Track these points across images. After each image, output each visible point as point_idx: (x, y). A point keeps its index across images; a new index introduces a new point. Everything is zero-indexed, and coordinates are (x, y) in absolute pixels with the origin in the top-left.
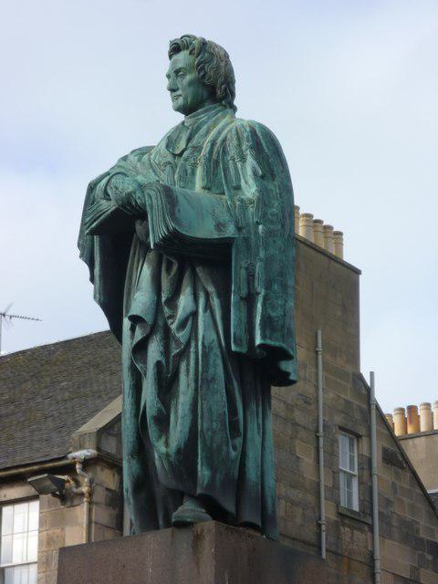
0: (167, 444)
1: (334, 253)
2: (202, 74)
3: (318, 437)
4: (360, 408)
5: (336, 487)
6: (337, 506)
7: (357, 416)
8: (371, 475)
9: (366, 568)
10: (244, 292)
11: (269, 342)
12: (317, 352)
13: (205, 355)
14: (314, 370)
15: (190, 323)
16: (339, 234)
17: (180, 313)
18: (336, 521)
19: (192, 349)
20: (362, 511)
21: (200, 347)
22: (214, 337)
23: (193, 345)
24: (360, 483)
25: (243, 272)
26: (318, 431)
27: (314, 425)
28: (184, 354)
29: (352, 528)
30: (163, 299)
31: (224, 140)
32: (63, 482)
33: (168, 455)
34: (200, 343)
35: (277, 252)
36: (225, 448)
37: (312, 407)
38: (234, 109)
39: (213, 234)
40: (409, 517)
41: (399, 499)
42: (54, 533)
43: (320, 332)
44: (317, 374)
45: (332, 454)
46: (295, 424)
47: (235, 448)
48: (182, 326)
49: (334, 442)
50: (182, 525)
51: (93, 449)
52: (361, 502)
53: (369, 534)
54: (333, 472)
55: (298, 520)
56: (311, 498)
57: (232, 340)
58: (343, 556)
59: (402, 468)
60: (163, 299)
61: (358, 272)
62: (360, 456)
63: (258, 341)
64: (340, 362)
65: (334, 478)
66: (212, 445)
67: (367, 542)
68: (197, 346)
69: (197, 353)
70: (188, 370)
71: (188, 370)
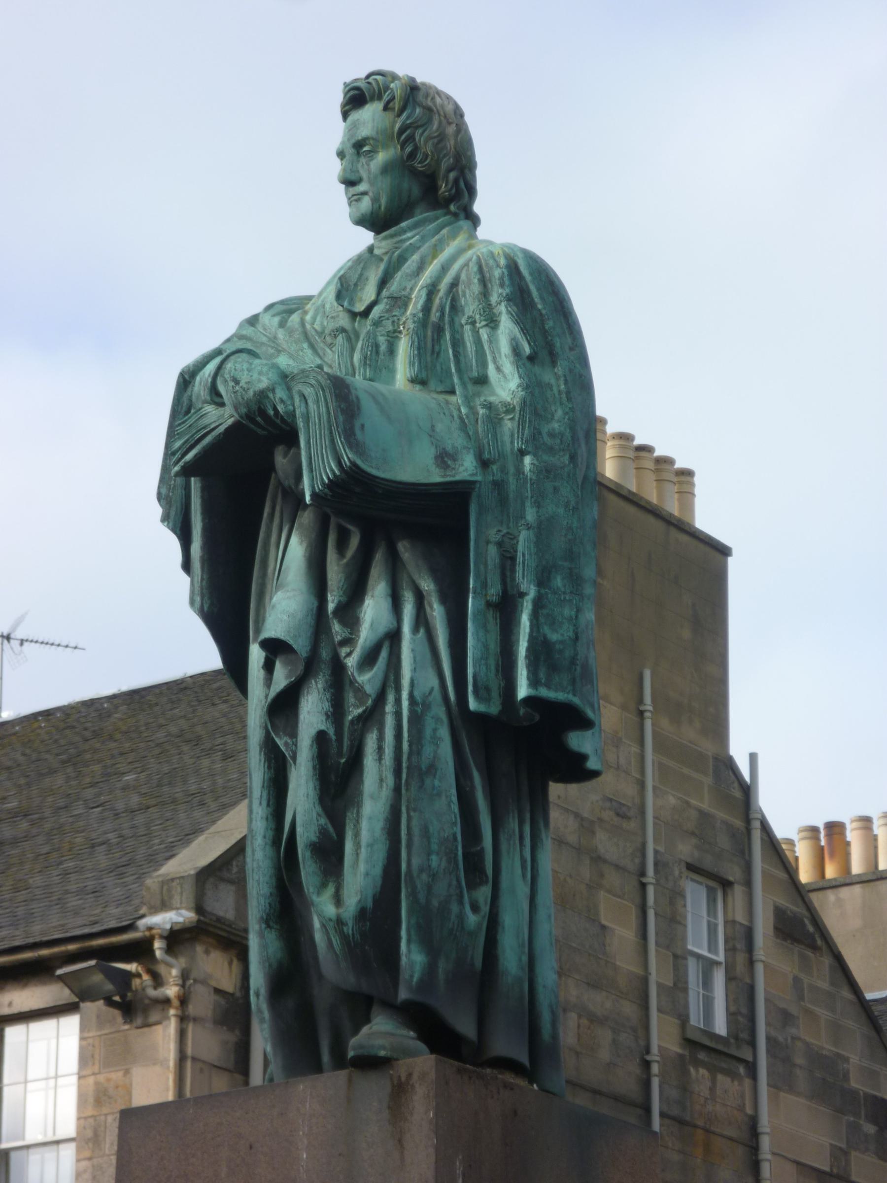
0: (338, 900)
1: (676, 513)
3: (643, 886)
5: (680, 985)
7: (724, 842)
8: (751, 963)
9: (740, 1151)
10: (494, 591)
11: (544, 692)
13: (416, 719)
14: (635, 749)
16: (687, 474)
17: (366, 635)
18: (681, 1056)
19: (389, 708)
20: (734, 1033)
21: (405, 704)
22: (434, 682)
23: (391, 698)
24: (730, 978)
25: (492, 552)
26: (643, 874)
27: (637, 861)
29: (713, 1070)
30: (331, 606)
31: (454, 284)
32: (129, 975)
33: (340, 922)
34: (405, 695)
35: (561, 511)
36: (455, 908)
37: (632, 825)
38: (475, 221)
39: (436, 477)
40: (825, 1044)
42: (108, 1080)
43: (647, 674)
44: (642, 758)
46: (597, 859)
47: (475, 908)
48: (369, 659)
49: (676, 896)
51: (188, 909)
52: (731, 1016)
53: (747, 1082)
54: (675, 956)
55: (605, 1054)
56: (629, 1009)
57: (470, 688)
58: (695, 1126)
59: (814, 948)
63: (523, 691)
68: (398, 701)
69: (398, 715)
70: (380, 749)
71: (380, 749)
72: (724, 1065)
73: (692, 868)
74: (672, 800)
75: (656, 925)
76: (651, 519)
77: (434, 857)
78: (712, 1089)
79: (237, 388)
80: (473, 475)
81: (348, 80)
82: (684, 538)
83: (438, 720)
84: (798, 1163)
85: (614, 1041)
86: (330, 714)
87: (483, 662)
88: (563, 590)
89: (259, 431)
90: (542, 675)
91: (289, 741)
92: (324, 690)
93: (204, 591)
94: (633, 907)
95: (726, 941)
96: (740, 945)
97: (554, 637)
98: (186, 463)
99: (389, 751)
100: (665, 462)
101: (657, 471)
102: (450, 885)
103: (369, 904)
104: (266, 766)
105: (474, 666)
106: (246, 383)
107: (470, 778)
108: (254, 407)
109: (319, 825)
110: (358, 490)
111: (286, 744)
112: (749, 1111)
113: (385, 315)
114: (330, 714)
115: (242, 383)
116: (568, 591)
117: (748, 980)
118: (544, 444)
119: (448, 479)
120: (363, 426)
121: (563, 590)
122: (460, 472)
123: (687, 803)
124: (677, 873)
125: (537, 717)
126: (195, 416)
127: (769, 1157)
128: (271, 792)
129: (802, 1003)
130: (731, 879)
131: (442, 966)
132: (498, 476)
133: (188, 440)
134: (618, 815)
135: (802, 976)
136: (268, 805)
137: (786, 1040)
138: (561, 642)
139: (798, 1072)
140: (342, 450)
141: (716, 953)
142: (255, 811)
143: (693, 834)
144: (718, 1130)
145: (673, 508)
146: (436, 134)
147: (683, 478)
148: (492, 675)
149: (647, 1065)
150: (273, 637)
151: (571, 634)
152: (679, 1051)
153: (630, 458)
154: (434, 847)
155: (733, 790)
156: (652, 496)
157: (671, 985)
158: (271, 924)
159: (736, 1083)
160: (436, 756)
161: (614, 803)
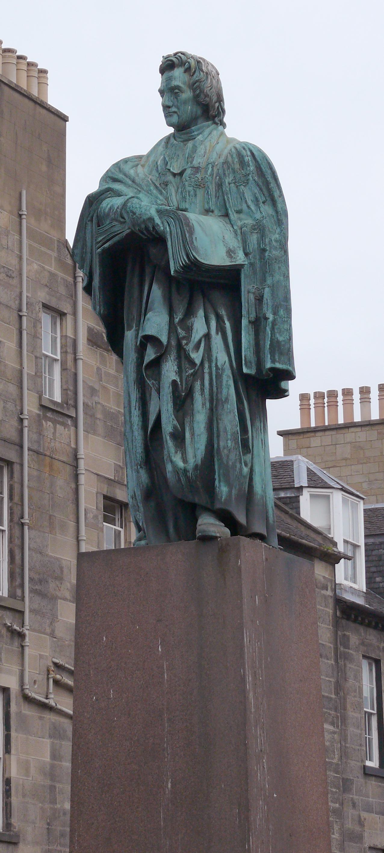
1: (15, 81)
2: (198, 92)
3: (20, 317)
4: (65, 280)
5: (38, 375)
6: (40, 398)
7: (62, 290)
8: (75, 360)
9: (68, 468)
10: (253, 316)
11: (273, 366)
12: (20, 216)
14: (17, 237)
15: (203, 344)
16: (44, 72)
18: (39, 415)
19: (206, 370)
20: (65, 402)
21: (214, 369)
22: (226, 359)
23: (206, 365)
24: (64, 369)
26: (20, 310)
27: (17, 302)
28: (198, 374)
29: (55, 422)
30: (177, 320)
34: (213, 365)
35: (282, 278)
36: (238, 465)
37: (15, 282)
38: (223, 125)
39: (227, 262)
41: (104, 387)
43: (24, 193)
44: (21, 242)
45: (35, 337)
47: (246, 465)
49: (36, 322)
50: (207, 539)
52: (64, 391)
53: (73, 429)
54: (36, 357)
56: (12, 389)
57: (243, 362)
58: (45, 455)
60: (177, 320)
61: (65, 119)
62: (64, 337)
64: (44, 227)
65: (36, 365)
66: (228, 462)
67: (70, 438)
68: (210, 367)
69: (210, 374)
70: (202, 390)
71: (202, 390)
72: (61, 420)
73: (46, 307)
74: (36, 267)
75: (27, 339)
76: (26, 101)
77: (229, 442)
78: (54, 433)
79: (134, 216)
80: (243, 261)
81: (165, 55)
82: (44, 111)
83: (228, 376)
84: (98, 475)
85: (4, 407)
86: (177, 372)
87: (248, 349)
88: (283, 316)
89: (143, 236)
90: (277, 357)
91: (154, 382)
92: (174, 360)
93: (101, 303)
94: (15, 329)
95: (61, 348)
96: (70, 350)
97: (281, 339)
98: (104, 248)
99: (207, 391)
100: (32, 65)
101: (39, 78)
102: (236, 455)
103: (199, 462)
104: (137, 391)
105: (245, 352)
106: (139, 214)
107: (243, 403)
108: (143, 226)
109: (173, 424)
110: (194, 269)
111: (153, 384)
112: (73, 446)
113: (191, 176)
114: (177, 372)
115: (137, 214)
116: (286, 316)
117: (73, 370)
118: (274, 246)
119: (233, 263)
120: (196, 238)
121: (283, 316)
122: (238, 260)
123: (43, 267)
124: (37, 308)
125: (272, 375)
126: (109, 225)
127: (84, 472)
128: (140, 403)
129: (101, 382)
130: (65, 311)
131: (234, 492)
132: (252, 261)
133: (105, 237)
134: (7, 276)
135: (101, 367)
136: (139, 410)
137: (93, 404)
138: (284, 341)
139: (98, 422)
140: (189, 251)
141: (56, 355)
142: (132, 412)
143: (46, 286)
144: (57, 457)
145: (35, 92)
146: (210, 85)
147: (41, 75)
148: (252, 355)
149: (21, 420)
150: (150, 334)
151: (288, 337)
152: (38, 412)
153: (36, 77)
154: (229, 437)
155: (67, 259)
156: (24, 85)
157: (34, 374)
158: (142, 466)
159: (66, 430)
160: (228, 394)
161: (5, 269)
